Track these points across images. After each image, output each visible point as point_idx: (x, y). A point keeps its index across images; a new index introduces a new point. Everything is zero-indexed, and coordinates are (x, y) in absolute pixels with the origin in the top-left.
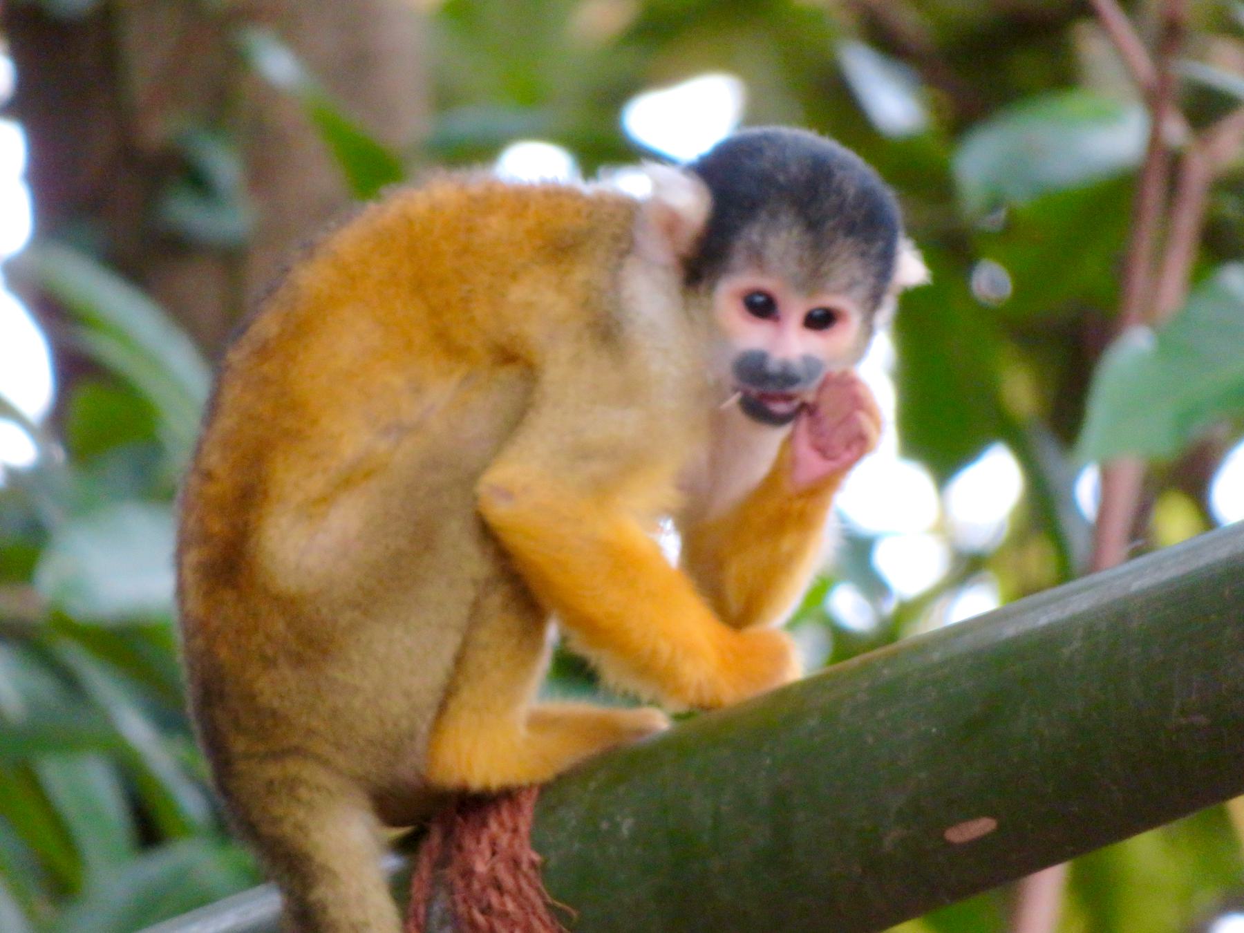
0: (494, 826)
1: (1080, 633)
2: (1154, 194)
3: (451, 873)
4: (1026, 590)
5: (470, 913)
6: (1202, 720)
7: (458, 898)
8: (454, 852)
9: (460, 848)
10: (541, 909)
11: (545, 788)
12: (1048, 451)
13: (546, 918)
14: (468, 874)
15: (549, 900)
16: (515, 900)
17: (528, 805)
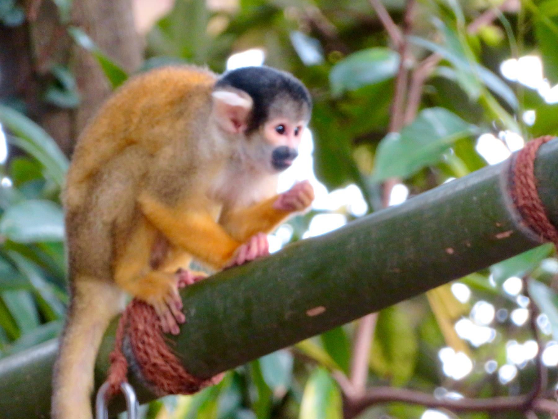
2: (401, 86)
3: (130, 330)
6: (397, 271)
14: (136, 330)
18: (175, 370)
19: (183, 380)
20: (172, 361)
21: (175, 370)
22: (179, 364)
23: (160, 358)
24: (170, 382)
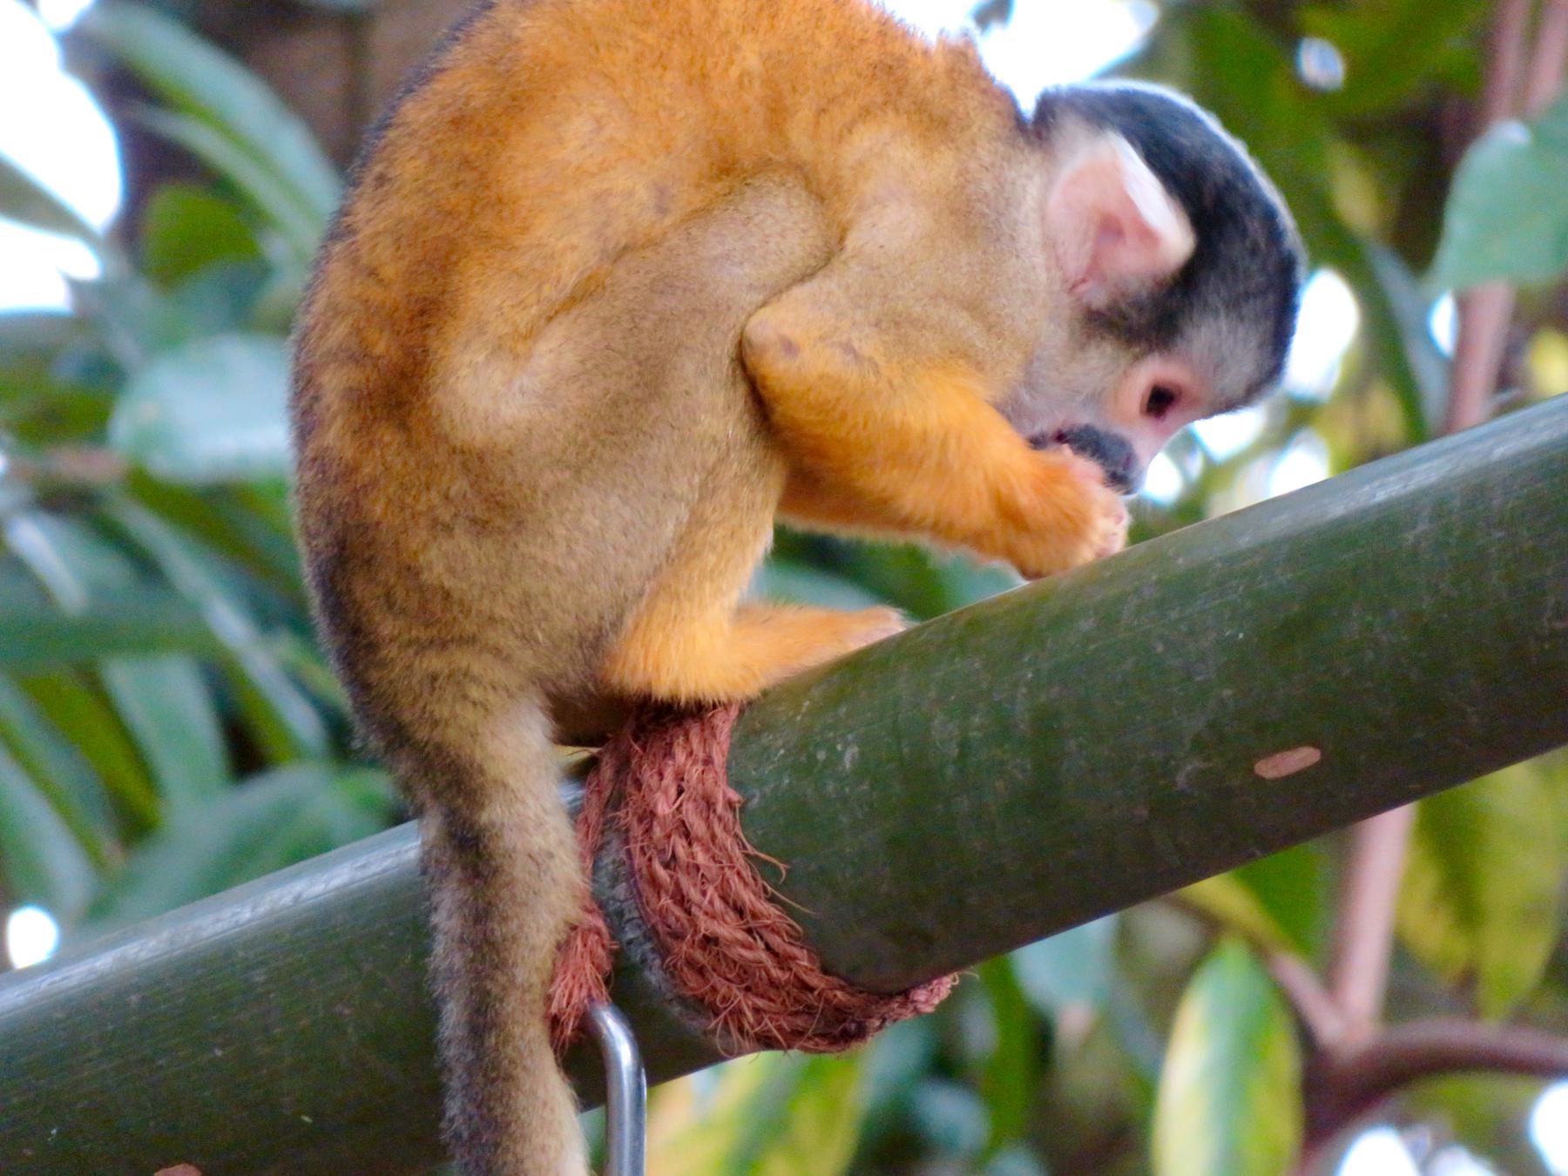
0: (680, 756)
1: (1426, 513)
3: (627, 816)
4: (1371, 453)
5: (650, 867)
7: (635, 847)
8: (631, 789)
9: (638, 784)
10: (740, 862)
11: (748, 706)
12: (1391, 272)
13: (746, 873)
14: (648, 816)
15: (751, 850)
16: (707, 850)
17: (724, 725)
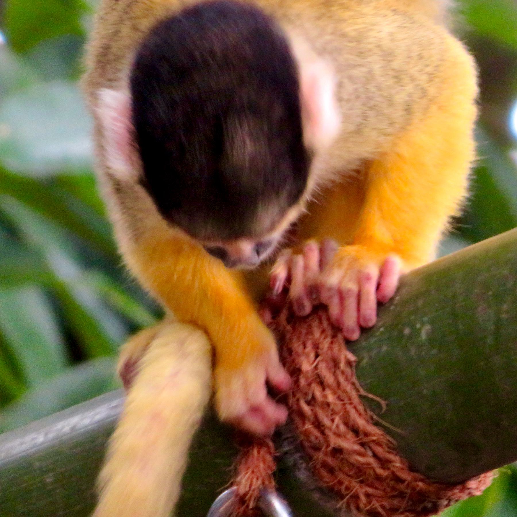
18: (384, 463)
19: (402, 487)
20: (378, 443)
21: (384, 463)
22: (392, 449)
23: (350, 435)
24: (370, 490)
